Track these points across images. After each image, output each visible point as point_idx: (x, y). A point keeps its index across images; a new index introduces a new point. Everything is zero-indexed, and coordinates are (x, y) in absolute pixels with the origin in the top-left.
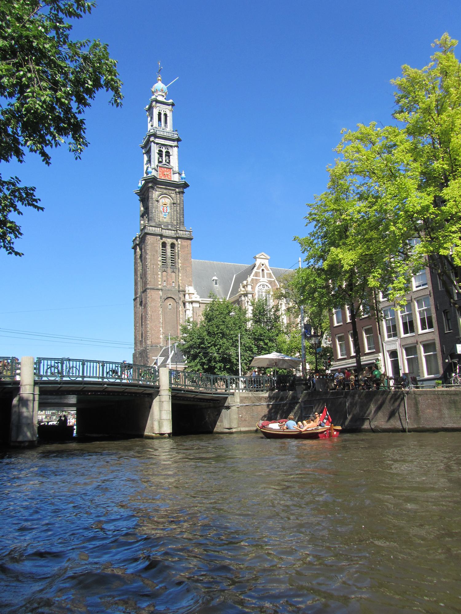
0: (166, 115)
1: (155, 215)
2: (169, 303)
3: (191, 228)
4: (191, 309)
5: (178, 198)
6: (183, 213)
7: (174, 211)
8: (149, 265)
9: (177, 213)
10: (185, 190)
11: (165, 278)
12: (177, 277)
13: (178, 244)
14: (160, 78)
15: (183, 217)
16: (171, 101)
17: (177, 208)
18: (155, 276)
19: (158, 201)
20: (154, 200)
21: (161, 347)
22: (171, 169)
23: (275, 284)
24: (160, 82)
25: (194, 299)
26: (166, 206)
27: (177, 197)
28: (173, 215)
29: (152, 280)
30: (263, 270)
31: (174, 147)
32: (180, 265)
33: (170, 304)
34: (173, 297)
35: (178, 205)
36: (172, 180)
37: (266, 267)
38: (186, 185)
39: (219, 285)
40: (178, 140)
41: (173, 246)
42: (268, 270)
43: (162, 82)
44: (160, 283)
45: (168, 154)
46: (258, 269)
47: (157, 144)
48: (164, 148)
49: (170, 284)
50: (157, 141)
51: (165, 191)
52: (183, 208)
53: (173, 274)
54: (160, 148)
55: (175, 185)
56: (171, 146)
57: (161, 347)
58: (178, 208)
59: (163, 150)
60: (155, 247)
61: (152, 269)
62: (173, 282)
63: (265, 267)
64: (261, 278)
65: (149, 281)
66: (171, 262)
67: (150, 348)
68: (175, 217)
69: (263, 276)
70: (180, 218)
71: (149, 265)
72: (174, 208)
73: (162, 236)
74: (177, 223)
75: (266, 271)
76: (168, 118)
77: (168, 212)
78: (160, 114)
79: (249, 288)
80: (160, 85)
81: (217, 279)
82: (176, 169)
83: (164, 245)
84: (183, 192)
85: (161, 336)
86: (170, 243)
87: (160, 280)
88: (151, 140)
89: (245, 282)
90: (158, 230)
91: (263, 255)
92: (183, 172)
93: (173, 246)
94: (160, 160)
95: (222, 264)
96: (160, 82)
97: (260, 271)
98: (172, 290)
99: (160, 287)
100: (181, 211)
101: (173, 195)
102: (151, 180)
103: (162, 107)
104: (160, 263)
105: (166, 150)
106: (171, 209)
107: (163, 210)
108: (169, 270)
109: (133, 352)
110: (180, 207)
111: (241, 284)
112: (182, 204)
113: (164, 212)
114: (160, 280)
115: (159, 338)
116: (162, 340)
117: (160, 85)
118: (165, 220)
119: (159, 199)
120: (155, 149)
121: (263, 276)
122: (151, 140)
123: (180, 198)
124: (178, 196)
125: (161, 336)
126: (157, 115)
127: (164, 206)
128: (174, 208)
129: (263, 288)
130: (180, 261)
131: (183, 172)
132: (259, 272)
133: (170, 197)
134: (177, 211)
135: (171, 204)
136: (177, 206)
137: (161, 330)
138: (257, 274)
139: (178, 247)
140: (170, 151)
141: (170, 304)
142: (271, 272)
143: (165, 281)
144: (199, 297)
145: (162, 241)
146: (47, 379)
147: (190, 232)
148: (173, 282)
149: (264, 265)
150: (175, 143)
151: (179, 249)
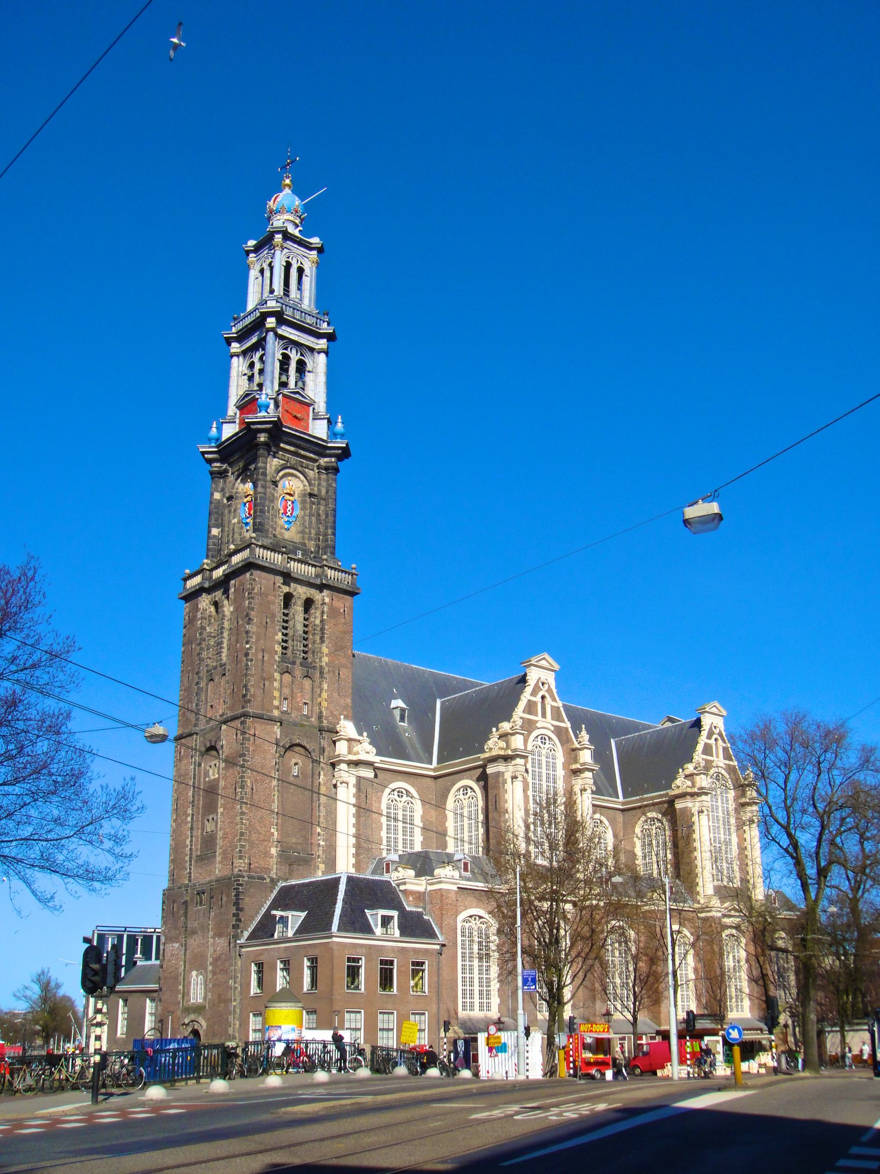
0: (301, 271)
1: (269, 518)
2: (294, 761)
3: (354, 566)
4: (352, 781)
5: (324, 484)
6: (334, 522)
7: (311, 515)
8: (253, 651)
9: (319, 521)
10: (341, 465)
11: (286, 691)
12: (315, 693)
13: (324, 604)
14: (288, 181)
15: (334, 534)
16: (315, 241)
17: (319, 509)
18: (267, 683)
19: (275, 483)
20: (268, 478)
21: (272, 880)
22: (309, 405)
23: (567, 738)
24: (287, 191)
25: (363, 757)
26: (291, 498)
27: (320, 479)
28: (307, 524)
29: (259, 692)
30: (543, 697)
31: (319, 353)
32: (326, 659)
33: (296, 764)
34: (305, 744)
35: (322, 502)
36: (310, 433)
37: (549, 690)
38: (345, 454)
39: (409, 722)
40: (331, 337)
41: (308, 603)
42: (554, 700)
43: (294, 192)
44: (276, 703)
45: (301, 367)
46: (534, 693)
47: (282, 337)
48: (294, 351)
49: (300, 709)
50: (286, 331)
51: (294, 459)
52: (334, 510)
53: (307, 683)
54: (286, 349)
55: (319, 448)
56: (312, 350)
57: (274, 882)
58: (322, 508)
59: (292, 356)
60: (269, 603)
61: (260, 664)
62: (306, 704)
63: (547, 691)
64: (539, 718)
65: (251, 695)
66: (302, 648)
67: (247, 883)
68: (313, 531)
69: (544, 715)
70: (326, 535)
71: (253, 651)
72: (311, 508)
73: (288, 577)
74: (318, 546)
75: (548, 700)
76: (304, 278)
77: (295, 514)
78: (288, 266)
79: (517, 742)
80: (286, 198)
81: (404, 706)
82: (321, 406)
83: (288, 599)
84: (336, 470)
85: (273, 851)
86: (304, 597)
87: (276, 694)
88: (268, 326)
89: (505, 726)
90: (277, 559)
91: (547, 659)
92: (340, 420)
93: (308, 603)
94: (284, 378)
95: (406, 667)
96: (287, 191)
97: (538, 699)
98: (302, 725)
99: (276, 713)
100: (331, 519)
101: (311, 474)
102: (268, 426)
103: (295, 250)
104: (278, 648)
105: (299, 356)
106: (303, 508)
107: (286, 508)
108: (298, 671)
109: (165, 884)
110: (326, 505)
111: (494, 729)
112: (333, 496)
113: (285, 513)
114: (276, 694)
115: (267, 854)
116: (275, 860)
117: (286, 198)
118: (287, 535)
119: (278, 478)
120: (275, 350)
121: (544, 715)
122: (268, 326)
123: (329, 485)
124: (324, 476)
125: (273, 851)
126: (283, 268)
127: (288, 497)
128: (311, 508)
129: (542, 746)
130: (325, 650)
131: (340, 420)
132: (535, 703)
133: (302, 477)
134: (319, 515)
135: (304, 495)
136: (319, 504)
137: (273, 834)
138: (530, 708)
139: (323, 612)
140: (306, 361)
141: (296, 764)
142: (560, 704)
143: (285, 699)
144: (374, 751)
145: (286, 589)
146: (565, 1000)
147: (353, 574)
148: (306, 704)
149: (546, 686)
150: (323, 343)
151: (325, 617)
